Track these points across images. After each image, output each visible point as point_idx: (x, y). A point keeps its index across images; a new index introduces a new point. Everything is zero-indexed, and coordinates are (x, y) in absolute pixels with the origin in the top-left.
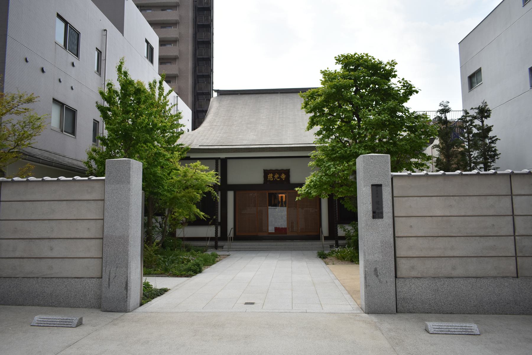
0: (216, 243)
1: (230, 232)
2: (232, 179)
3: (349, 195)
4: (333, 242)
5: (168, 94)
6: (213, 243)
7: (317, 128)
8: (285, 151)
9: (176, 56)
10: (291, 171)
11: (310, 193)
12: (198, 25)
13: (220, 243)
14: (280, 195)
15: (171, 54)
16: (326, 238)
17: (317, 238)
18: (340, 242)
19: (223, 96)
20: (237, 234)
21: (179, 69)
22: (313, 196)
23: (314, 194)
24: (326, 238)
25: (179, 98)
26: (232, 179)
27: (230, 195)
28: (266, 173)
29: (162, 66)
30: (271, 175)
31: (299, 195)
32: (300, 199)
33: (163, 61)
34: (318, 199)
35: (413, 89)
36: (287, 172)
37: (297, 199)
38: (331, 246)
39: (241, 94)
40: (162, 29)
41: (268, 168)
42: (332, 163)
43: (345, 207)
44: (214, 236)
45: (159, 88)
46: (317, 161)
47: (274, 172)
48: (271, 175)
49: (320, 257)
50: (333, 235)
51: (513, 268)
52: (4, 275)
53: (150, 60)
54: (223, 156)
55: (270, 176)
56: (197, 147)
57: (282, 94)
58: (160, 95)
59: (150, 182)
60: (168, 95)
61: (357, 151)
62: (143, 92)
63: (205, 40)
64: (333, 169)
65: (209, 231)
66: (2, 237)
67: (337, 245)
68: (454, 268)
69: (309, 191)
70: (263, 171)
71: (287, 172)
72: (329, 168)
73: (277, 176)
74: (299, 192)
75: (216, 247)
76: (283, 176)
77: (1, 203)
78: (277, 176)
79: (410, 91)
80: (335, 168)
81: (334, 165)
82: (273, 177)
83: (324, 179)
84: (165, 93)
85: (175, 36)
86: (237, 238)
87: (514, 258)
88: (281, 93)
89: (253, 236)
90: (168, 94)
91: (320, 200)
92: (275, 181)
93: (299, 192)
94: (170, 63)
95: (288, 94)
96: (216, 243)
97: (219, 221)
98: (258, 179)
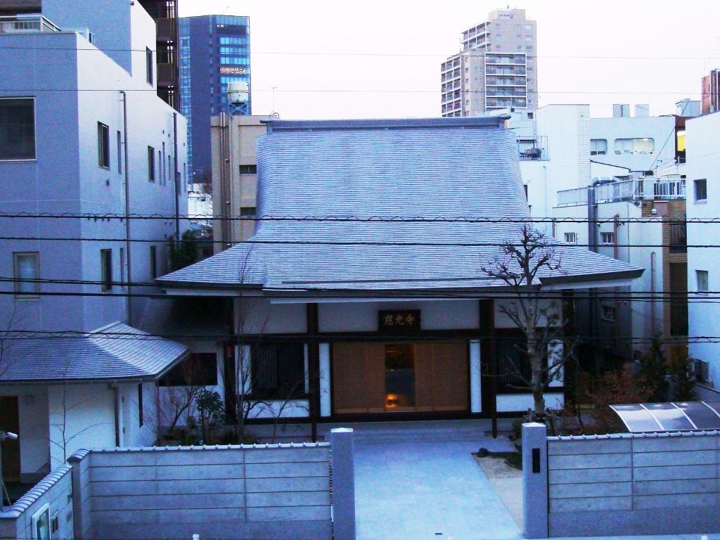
1: (325, 411)
2: (326, 325)
26: (326, 325)
28: (382, 314)
30: (391, 317)
47: (394, 313)
48: (391, 317)
51: (629, 504)
52: (3, 536)
55: (389, 318)
59: (232, 328)
65: (297, 409)
66: (719, 248)
68: (589, 506)
71: (417, 313)
73: (399, 318)
76: (410, 319)
77: (687, 224)
82: (394, 320)
87: (630, 470)
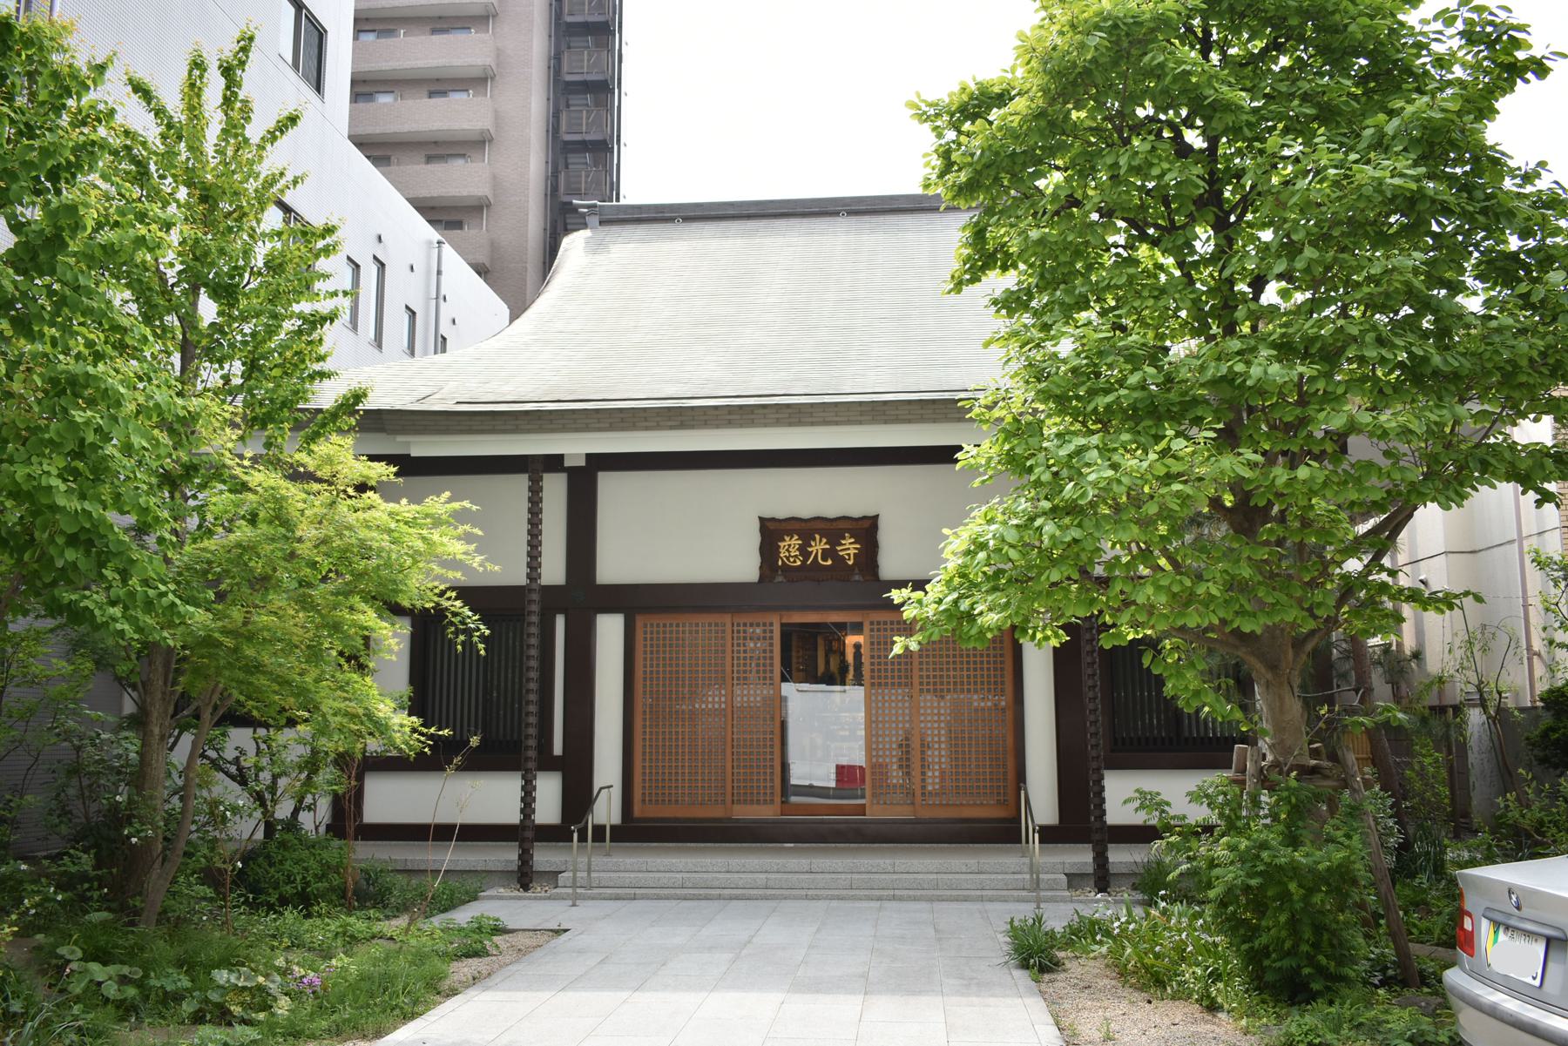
0: (525, 858)
1: (606, 810)
2: (616, 564)
3: (1192, 621)
4: (1081, 857)
5: (272, 137)
6: (507, 855)
7: (1000, 282)
8: (849, 422)
9: (482, 132)
10: (882, 523)
11: (970, 617)
12: (569, 25)
13: (544, 857)
14: (851, 640)
15: (466, 126)
16: (1049, 835)
17: (1003, 831)
18: (1121, 857)
19: (615, 229)
20: (638, 811)
21: (494, 177)
22: (982, 632)
23: (992, 619)
24: (1049, 835)
25: (447, 248)
27: (609, 630)
28: (772, 531)
29: (361, 105)
30: (795, 542)
31: (908, 629)
32: (914, 646)
33: (363, 88)
34: (1010, 646)
35: (1521, 55)
36: (867, 530)
37: (897, 649)
38: (1074, 880)
39: (687, 219)
40: (438, 39)
41: (781, 509)
42: (1095, 440)
43: (1169, 689)
44: (514, 817)
45: (228, 102)
46: (1009, 435)
47: (806, 528)
48: (795, 542)
49: (1025, 965)
50: (1080, 819)
53: (306, 77)
54: (575, 447)
55: (789, 548)
56: (450, 406)
57: (854, 219)
58: (232, 130)
60: (274, 139)
61: (1240, 367)
62: (28, 42)
63: (589, 78)
64: (1098, 473)
65: (492, 797)
67: (1102, 879)
69: (965, 605)
70: (757, 525)
71: (867, 530)
72: (1073, 466)
73: (818, 546)
74: (909, 613)
75: (524, 877)
76: (849, 548)
78: (818, 546)
79: (1505, 61)
80: (1115, 466)
81: (1104, 450)
83: (1050, 528)
84: (254, 132)
85: (479, 62)
86: (635, 830)
88: (851, 213)
89: (718, 817)
90: (272, 137)
91: (1017, 651)
92: (810, 572)
93: (909, 613)
94: (463, 156)
95: (881, 219)
96: (525, 858)
97: (558, 749)
98: (738, 562)
